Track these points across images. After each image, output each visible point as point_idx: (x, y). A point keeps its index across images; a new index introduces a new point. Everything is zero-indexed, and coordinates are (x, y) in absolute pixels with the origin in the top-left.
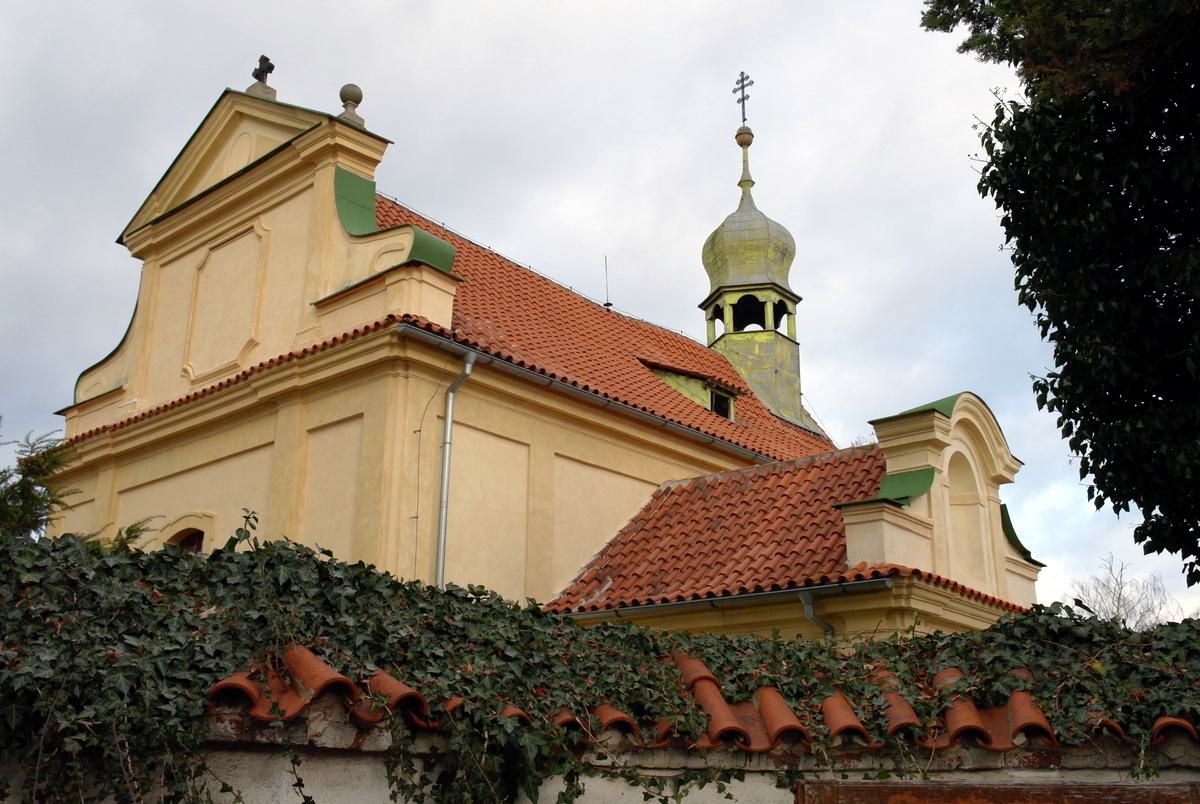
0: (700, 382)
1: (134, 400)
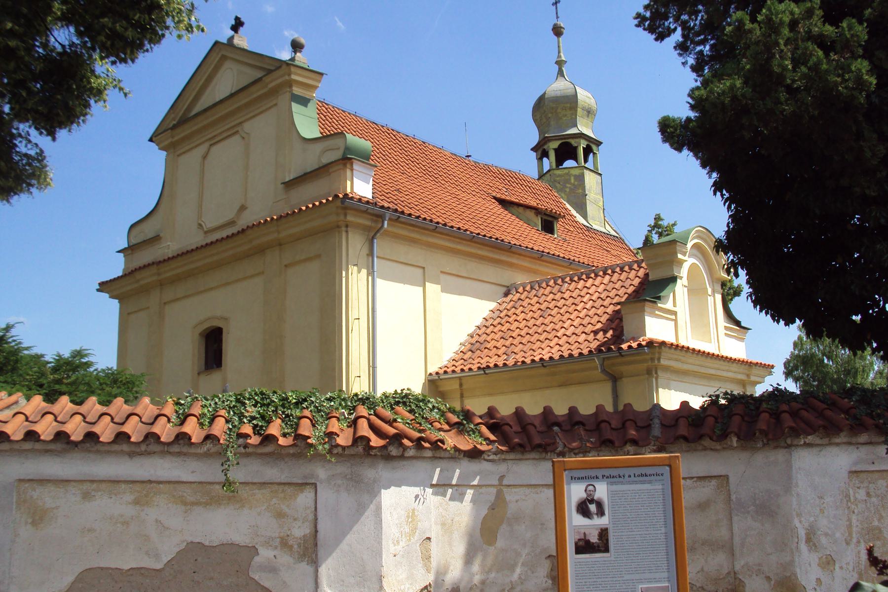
0: (534, 211)
1: (169, 243)
